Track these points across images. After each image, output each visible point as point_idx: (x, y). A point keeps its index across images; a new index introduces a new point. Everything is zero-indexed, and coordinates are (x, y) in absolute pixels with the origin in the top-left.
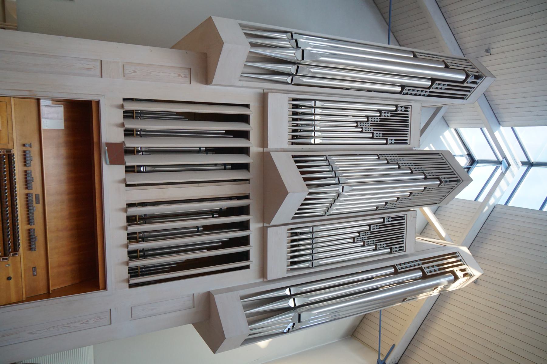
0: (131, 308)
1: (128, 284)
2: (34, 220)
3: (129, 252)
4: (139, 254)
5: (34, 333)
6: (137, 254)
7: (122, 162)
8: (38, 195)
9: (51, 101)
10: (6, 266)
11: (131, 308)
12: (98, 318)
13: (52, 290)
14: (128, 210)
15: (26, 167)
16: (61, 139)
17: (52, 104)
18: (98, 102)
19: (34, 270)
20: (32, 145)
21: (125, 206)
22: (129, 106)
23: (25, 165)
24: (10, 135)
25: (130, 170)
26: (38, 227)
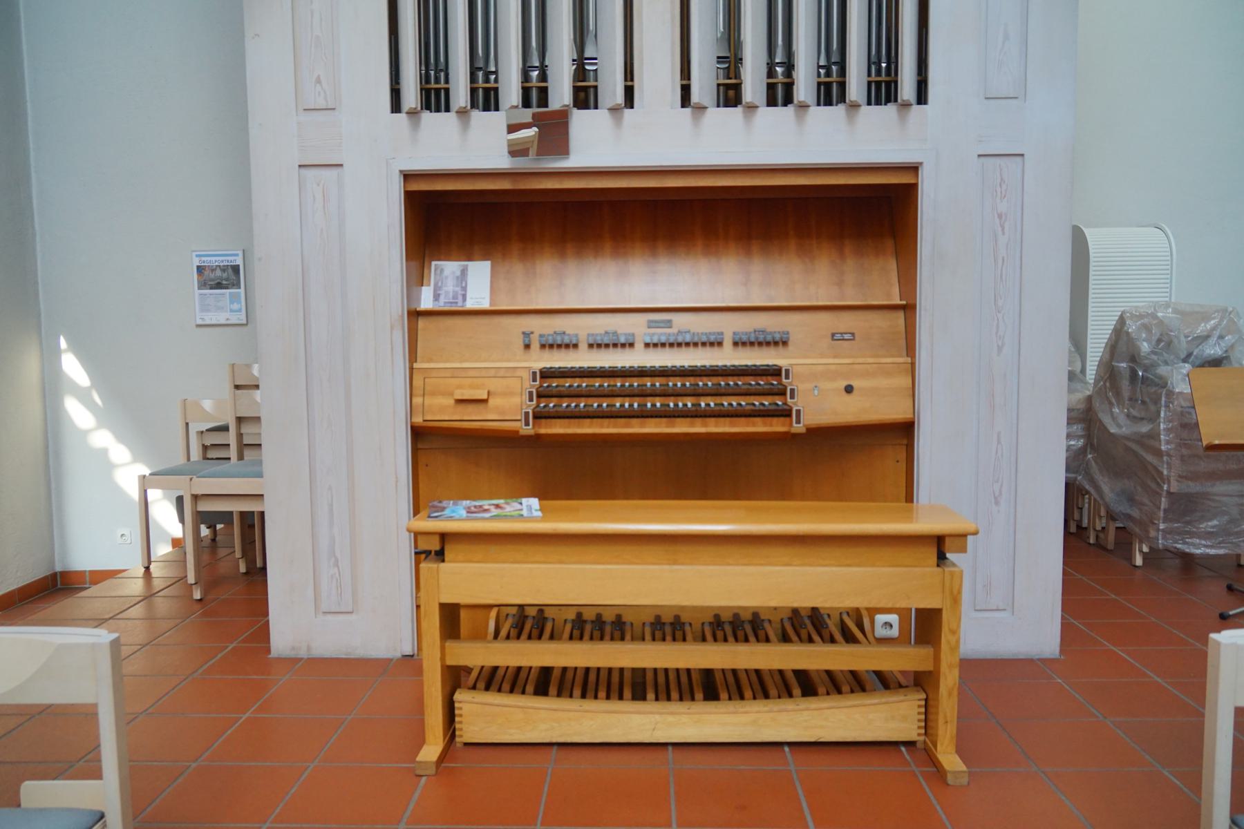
0: (986, 98)
1: (916, 108)
2: (710, 333)
3: (771, 102)
4: (835, 77)
5: (1000, 344)
6: (835, 84)
7: (562, 118)
8: (650, 322)
9: (423, 288)
10: (816, 394)
11: (986, 98)
12: (998, 186)
13: (901, 300)
14: (695, 101)
15: (580, 345)
16: (517, 268)
17: (429, 285)
18: (407, 176)
19: (838, 337)
20: (527, 330)
21: (688, 110)
22: (411, 95)
23: (576, 346)
24: (502, 373)
25: (585, 97)
26: (730, 325)
